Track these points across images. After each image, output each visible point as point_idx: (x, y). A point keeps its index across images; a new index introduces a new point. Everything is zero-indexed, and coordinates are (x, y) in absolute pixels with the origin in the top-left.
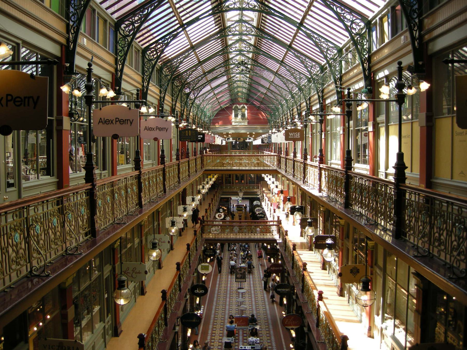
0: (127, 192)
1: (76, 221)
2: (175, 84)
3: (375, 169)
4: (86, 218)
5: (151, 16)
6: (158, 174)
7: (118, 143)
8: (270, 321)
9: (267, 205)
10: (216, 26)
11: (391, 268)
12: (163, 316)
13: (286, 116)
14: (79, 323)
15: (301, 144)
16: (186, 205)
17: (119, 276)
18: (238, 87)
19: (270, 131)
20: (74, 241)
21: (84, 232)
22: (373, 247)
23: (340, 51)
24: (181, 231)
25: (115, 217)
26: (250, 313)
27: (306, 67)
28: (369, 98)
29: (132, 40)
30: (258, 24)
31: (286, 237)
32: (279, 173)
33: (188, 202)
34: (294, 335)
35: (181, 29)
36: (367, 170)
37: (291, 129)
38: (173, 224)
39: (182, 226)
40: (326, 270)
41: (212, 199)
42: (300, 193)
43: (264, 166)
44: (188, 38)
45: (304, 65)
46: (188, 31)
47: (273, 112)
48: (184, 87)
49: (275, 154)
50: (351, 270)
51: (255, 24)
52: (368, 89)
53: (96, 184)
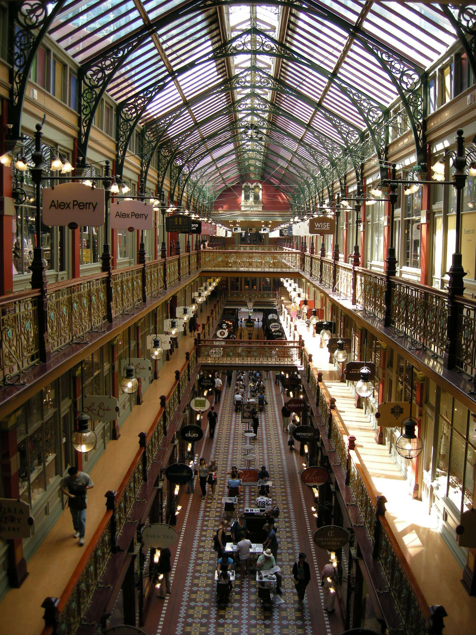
0: (90, 301)
1: (18, 339)
2: (163, 153)
3: (428, 276)
4: (32, 335)
5: (128, 60)
6: (134, 276)
7: (82, 233)
8: (287, 476)
9: (286, 320)
10: (218, 75)
11: (444, 407)
12: (140, 467)
13: (314, 199)
14: (26, 477)
15: (332, 238)
16: (176, 318)
17: (80, 413)
18: (250, 158)
19: (292, 220)
20: (15, 368)
21: (30, 354)
22: (424, 379)
23: (386, 112)
24: (169, 354)
25: (74, 334)
26: (260, 465)
27: (340, 133)
28: (422, 178)
29: (102, 92)
30: (276, 74)
31: (310, 363)
32: (303, 277)
33: (178, 315)
34: (317, 495)
35: (170, 78)
36: (417, 275)
37: (319, 218)
38: (156, 344)
39: (168, 347)
40: (362, 408)
41: (212, 311)
42: (330, 304)
43: (282, 267)
44: (181, 91)
45: (338, 130)
46: (180, 81)
47: (297, 193)
48: (175, 158)
49: (297, 251)
50: (392, 409)
51: (272, 73)
52: (422, 166)
53: (46, 290)
